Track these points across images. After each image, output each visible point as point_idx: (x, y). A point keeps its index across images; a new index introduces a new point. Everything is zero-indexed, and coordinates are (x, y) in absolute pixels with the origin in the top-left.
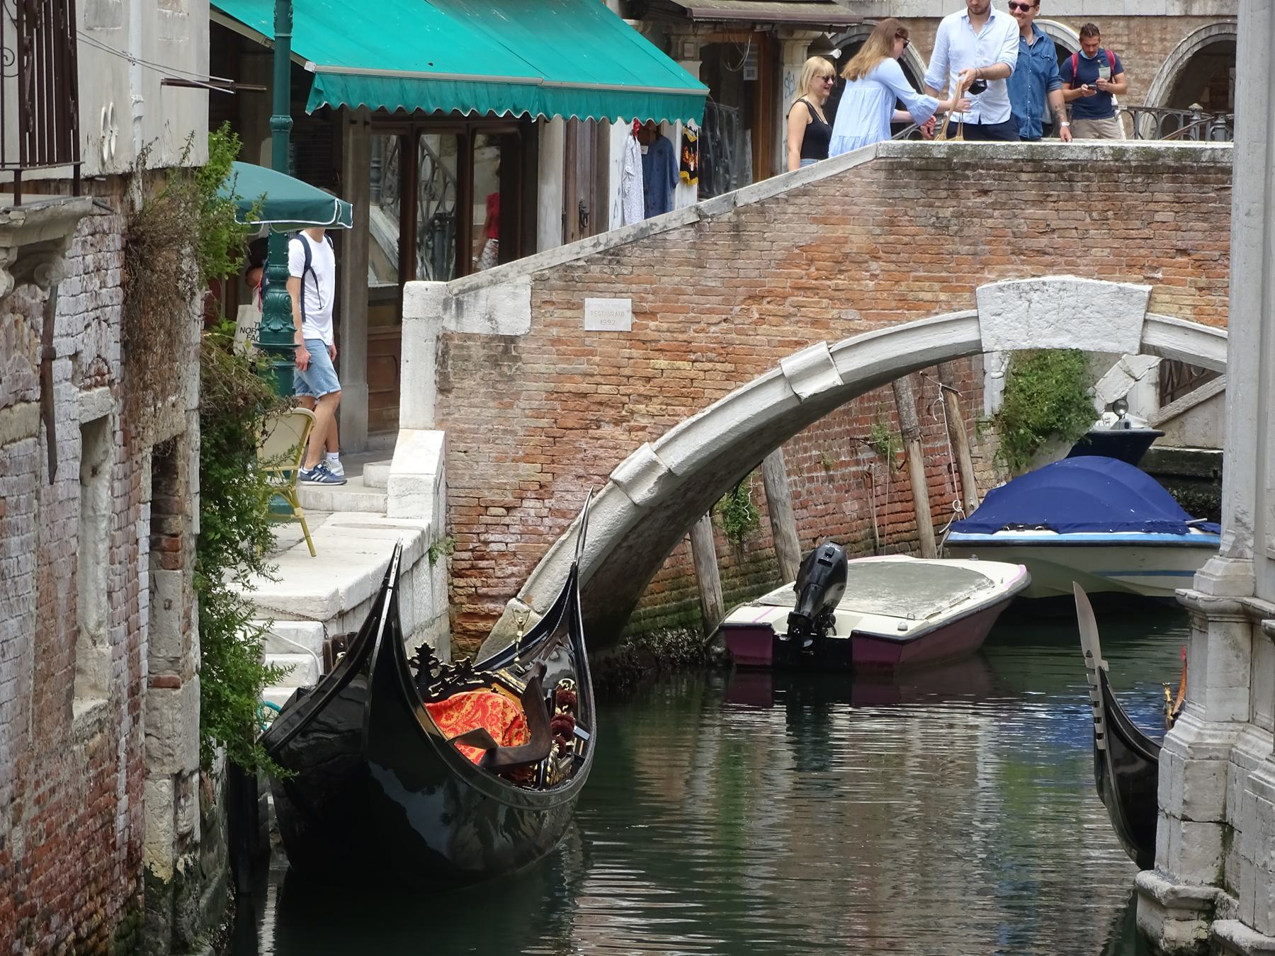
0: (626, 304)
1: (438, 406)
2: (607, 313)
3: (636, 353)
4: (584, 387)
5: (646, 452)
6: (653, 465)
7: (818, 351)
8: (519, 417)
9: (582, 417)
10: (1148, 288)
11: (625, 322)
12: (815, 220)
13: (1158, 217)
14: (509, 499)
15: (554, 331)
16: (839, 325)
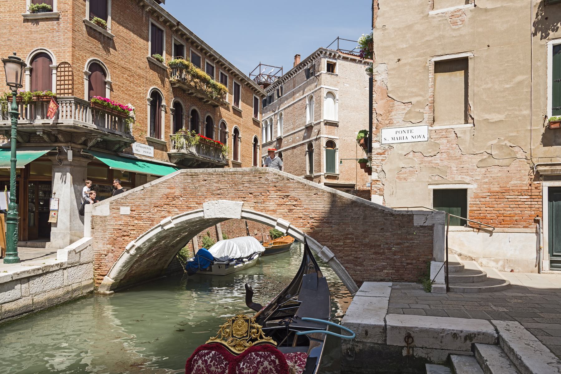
0: (129, 208)
1: (92, 232)
2: (125, 210)
3: (131, 220)
4: (121, 227)
5: (133, 243)
6: (133, 246)
7: (169, 219)
8: (108, 235)
9: (123, 234)
10: (243, 202)
11: (129, 212)
12: (168, 188)
13: (245, 185)
14: (106, 253)
15: (114, 215)
16: (174, 212)
